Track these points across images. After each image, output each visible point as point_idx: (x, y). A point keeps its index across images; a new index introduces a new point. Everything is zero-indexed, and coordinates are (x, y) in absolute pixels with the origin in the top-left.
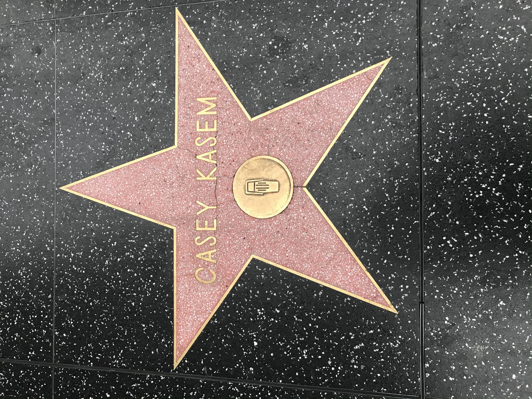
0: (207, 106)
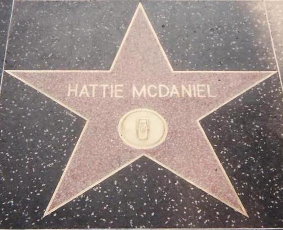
0: (139, 91)
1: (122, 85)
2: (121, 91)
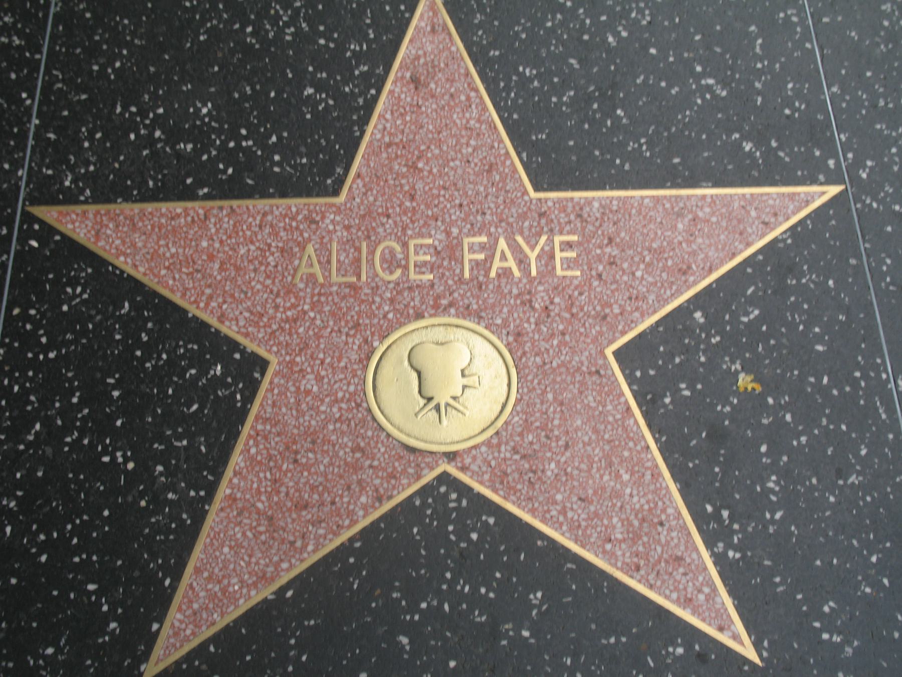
1: (574, 238)
2: (572, 254)
